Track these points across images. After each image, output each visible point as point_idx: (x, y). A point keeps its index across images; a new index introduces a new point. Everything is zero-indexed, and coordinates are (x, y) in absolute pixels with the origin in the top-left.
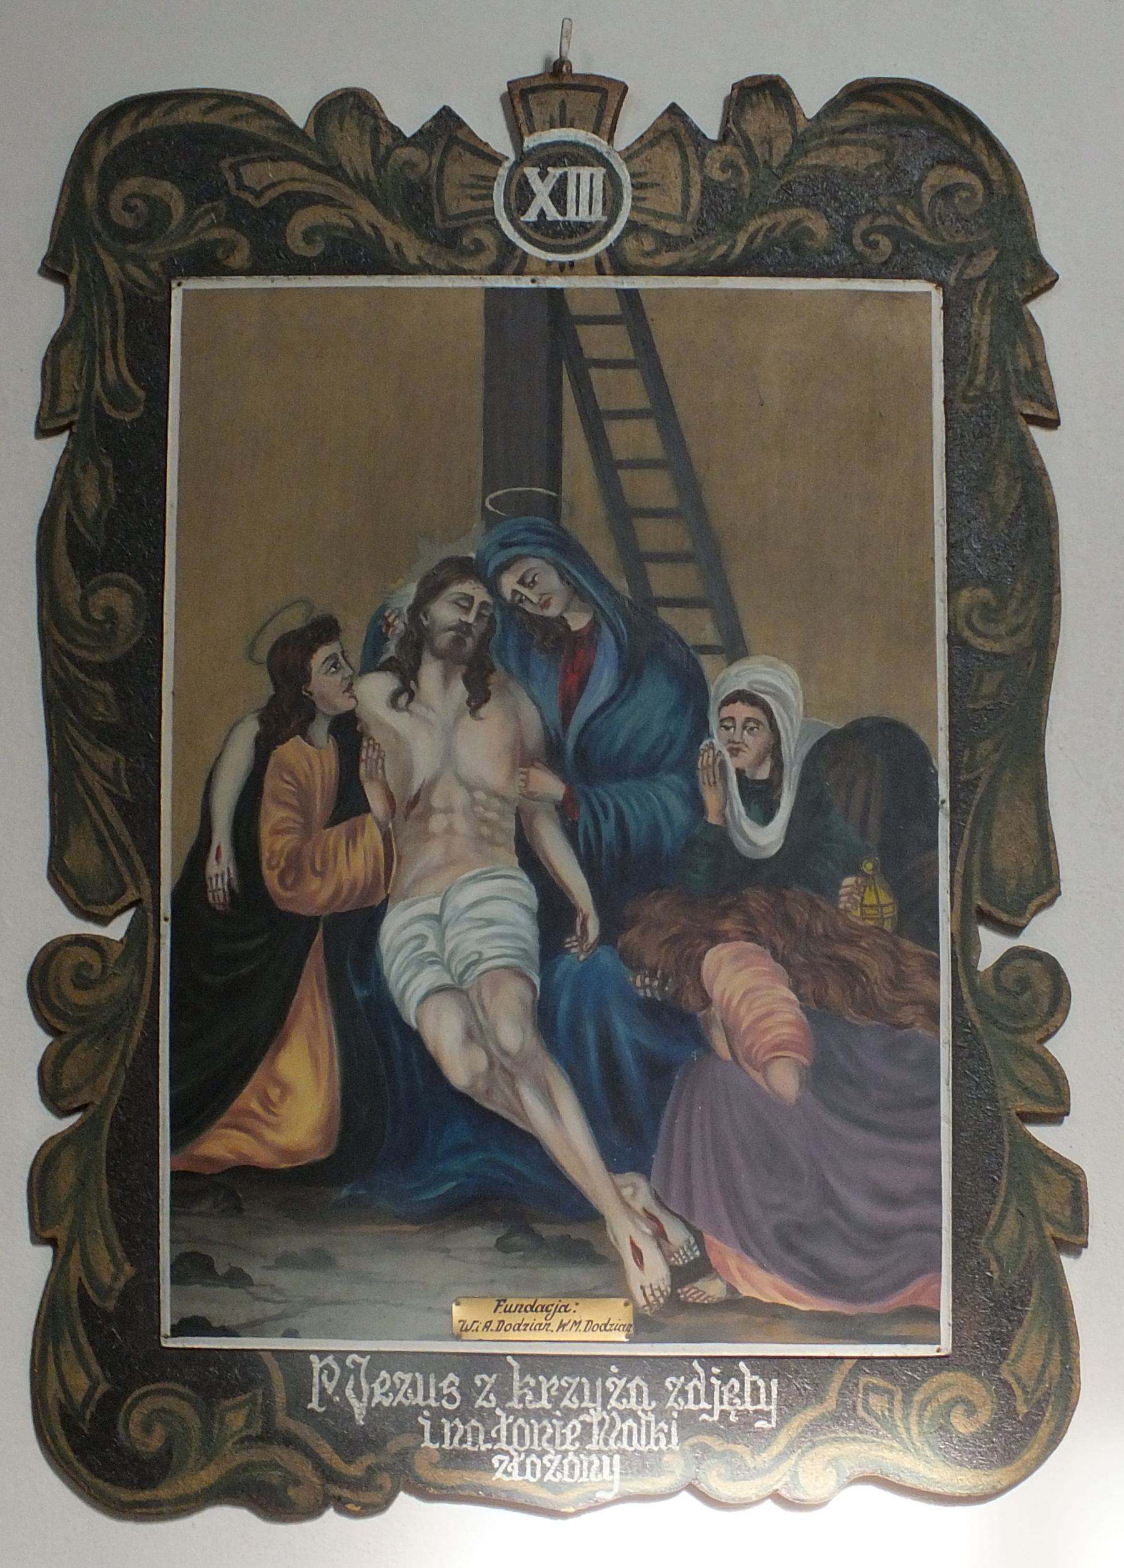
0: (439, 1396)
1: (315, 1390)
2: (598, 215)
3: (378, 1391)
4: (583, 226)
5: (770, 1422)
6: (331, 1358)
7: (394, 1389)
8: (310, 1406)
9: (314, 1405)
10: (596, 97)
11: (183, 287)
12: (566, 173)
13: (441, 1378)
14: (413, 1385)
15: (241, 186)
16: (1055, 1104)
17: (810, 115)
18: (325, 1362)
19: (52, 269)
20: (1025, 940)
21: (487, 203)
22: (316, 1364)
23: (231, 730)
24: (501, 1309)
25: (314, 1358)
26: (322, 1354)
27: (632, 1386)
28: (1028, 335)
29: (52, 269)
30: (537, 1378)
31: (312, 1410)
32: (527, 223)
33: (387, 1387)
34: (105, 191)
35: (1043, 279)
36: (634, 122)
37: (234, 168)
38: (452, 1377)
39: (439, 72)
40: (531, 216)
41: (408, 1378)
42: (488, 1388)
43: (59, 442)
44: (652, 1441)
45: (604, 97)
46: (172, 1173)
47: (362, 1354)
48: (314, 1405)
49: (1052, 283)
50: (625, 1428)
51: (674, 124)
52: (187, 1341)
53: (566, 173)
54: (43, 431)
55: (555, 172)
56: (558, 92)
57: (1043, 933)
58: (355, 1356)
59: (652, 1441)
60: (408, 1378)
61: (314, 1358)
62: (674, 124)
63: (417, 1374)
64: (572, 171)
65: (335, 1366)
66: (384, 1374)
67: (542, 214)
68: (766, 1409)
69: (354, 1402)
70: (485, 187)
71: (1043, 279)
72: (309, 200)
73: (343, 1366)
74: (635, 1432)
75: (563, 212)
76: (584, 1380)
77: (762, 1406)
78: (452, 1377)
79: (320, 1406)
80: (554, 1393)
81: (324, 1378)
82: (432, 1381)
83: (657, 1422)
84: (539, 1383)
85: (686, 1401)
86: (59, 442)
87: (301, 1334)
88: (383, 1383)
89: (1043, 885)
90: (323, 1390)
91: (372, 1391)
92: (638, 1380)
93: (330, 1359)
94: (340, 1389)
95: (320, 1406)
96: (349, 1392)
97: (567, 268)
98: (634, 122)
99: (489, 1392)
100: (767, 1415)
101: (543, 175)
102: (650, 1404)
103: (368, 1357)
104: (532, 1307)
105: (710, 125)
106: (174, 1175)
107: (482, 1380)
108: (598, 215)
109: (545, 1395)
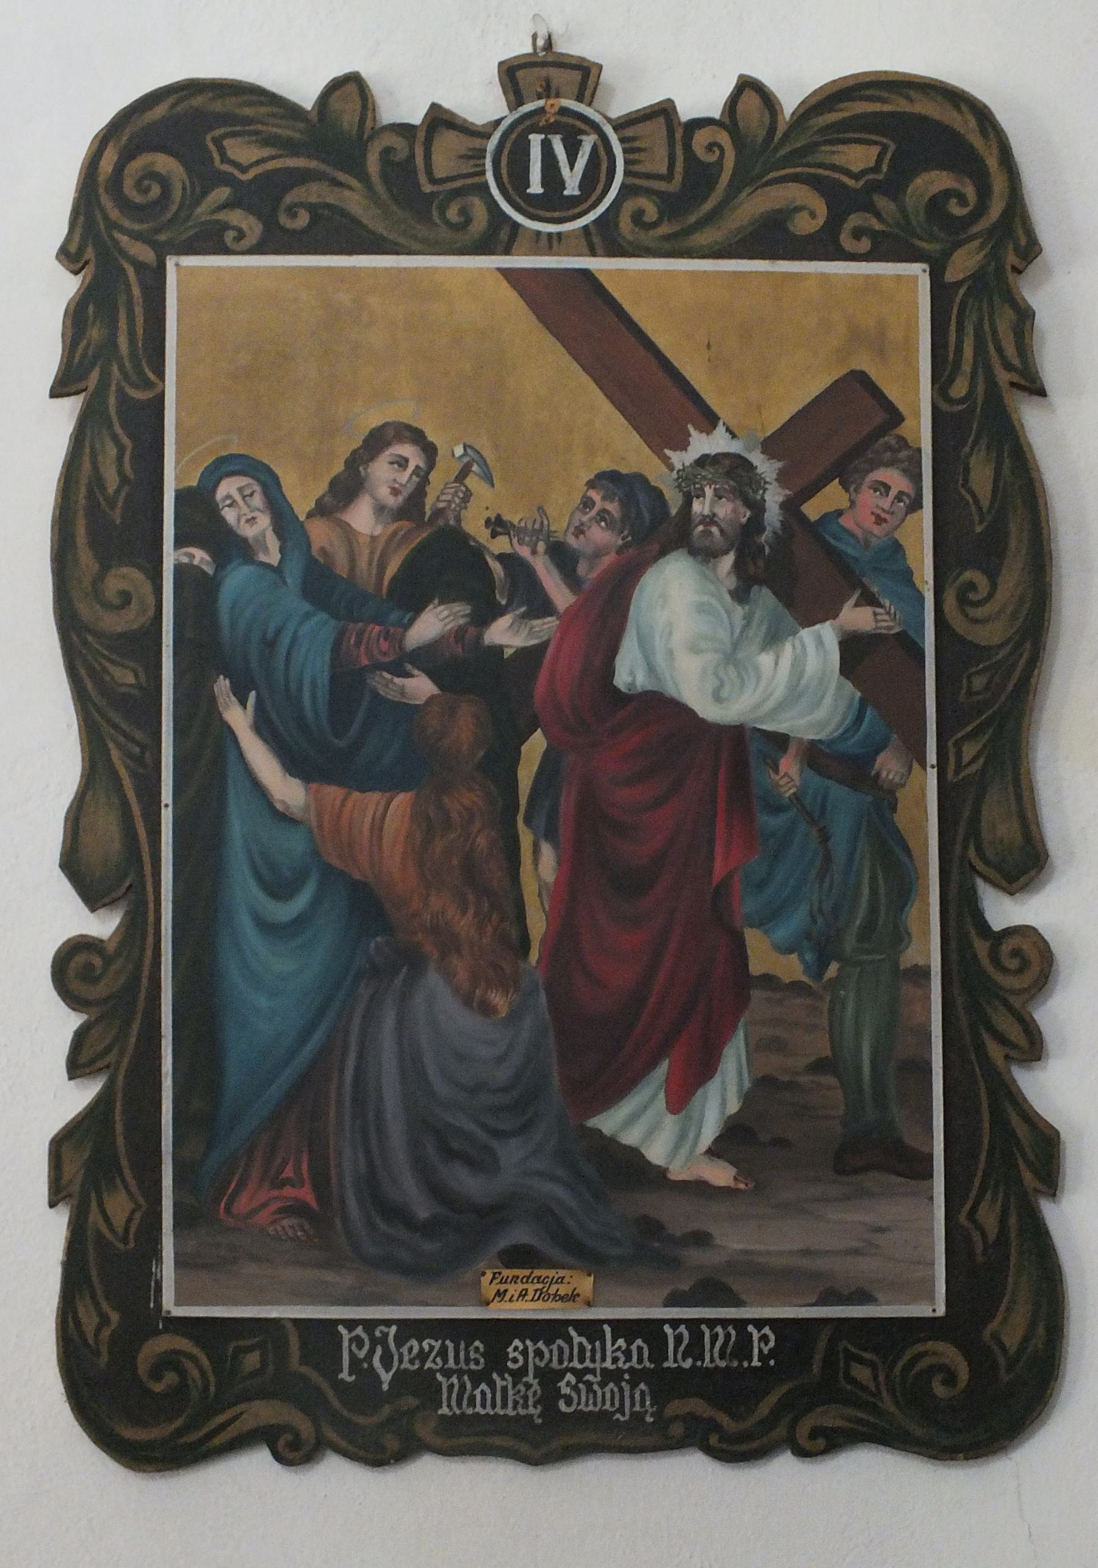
0: (468, 1360)
3: (406, 1359)
6: (360, 1328)
7: (423, 1356)
8: (666, 1365)
9: (344, 1375)
14: (443, 1353)
15: (224, 159)
18: (354, 1334)
22: (756, 1336)
24: (495, 1282)
26: (351, 1324)
29: (69, 256)
30: (524, 1343)
31: (342, 1380)
37: (218, 142)
38: (477, 1343)
41: (437, 1345)
44: (510, 1404)
45: (586, 75)
46: (932, 1176)
47: (388, 1323)
48: (344, 1375)
50: (477, 1392)
58: (383, 1328)
59: (510, 1404)
60: (437, 1345)
63: (448, 1342)
65: (364, 1336)
66: (414, 1343)
68: (591, 1366)
69: (381, 1371)
70: (479, 165)
72: (304, 177)
74: (489, 1396)
77: (588, 1363)
78: (477, 1343)
79: (350, 1374)
81: (354, 1347)
82: (462, 1345)
83: (514, 1385)
84: (526, 1348)
85: (445, 1361)
87: (879, 1296)
90: (760, 1351)
91: (401, 1356)
93: (359, 1331)
95: (350, 1374)
96: (376, 1361)
97: (544, 242)
103: (394, 1329)
104: (528, 1278)
106: (930, 1175)
107: (430, 1345)
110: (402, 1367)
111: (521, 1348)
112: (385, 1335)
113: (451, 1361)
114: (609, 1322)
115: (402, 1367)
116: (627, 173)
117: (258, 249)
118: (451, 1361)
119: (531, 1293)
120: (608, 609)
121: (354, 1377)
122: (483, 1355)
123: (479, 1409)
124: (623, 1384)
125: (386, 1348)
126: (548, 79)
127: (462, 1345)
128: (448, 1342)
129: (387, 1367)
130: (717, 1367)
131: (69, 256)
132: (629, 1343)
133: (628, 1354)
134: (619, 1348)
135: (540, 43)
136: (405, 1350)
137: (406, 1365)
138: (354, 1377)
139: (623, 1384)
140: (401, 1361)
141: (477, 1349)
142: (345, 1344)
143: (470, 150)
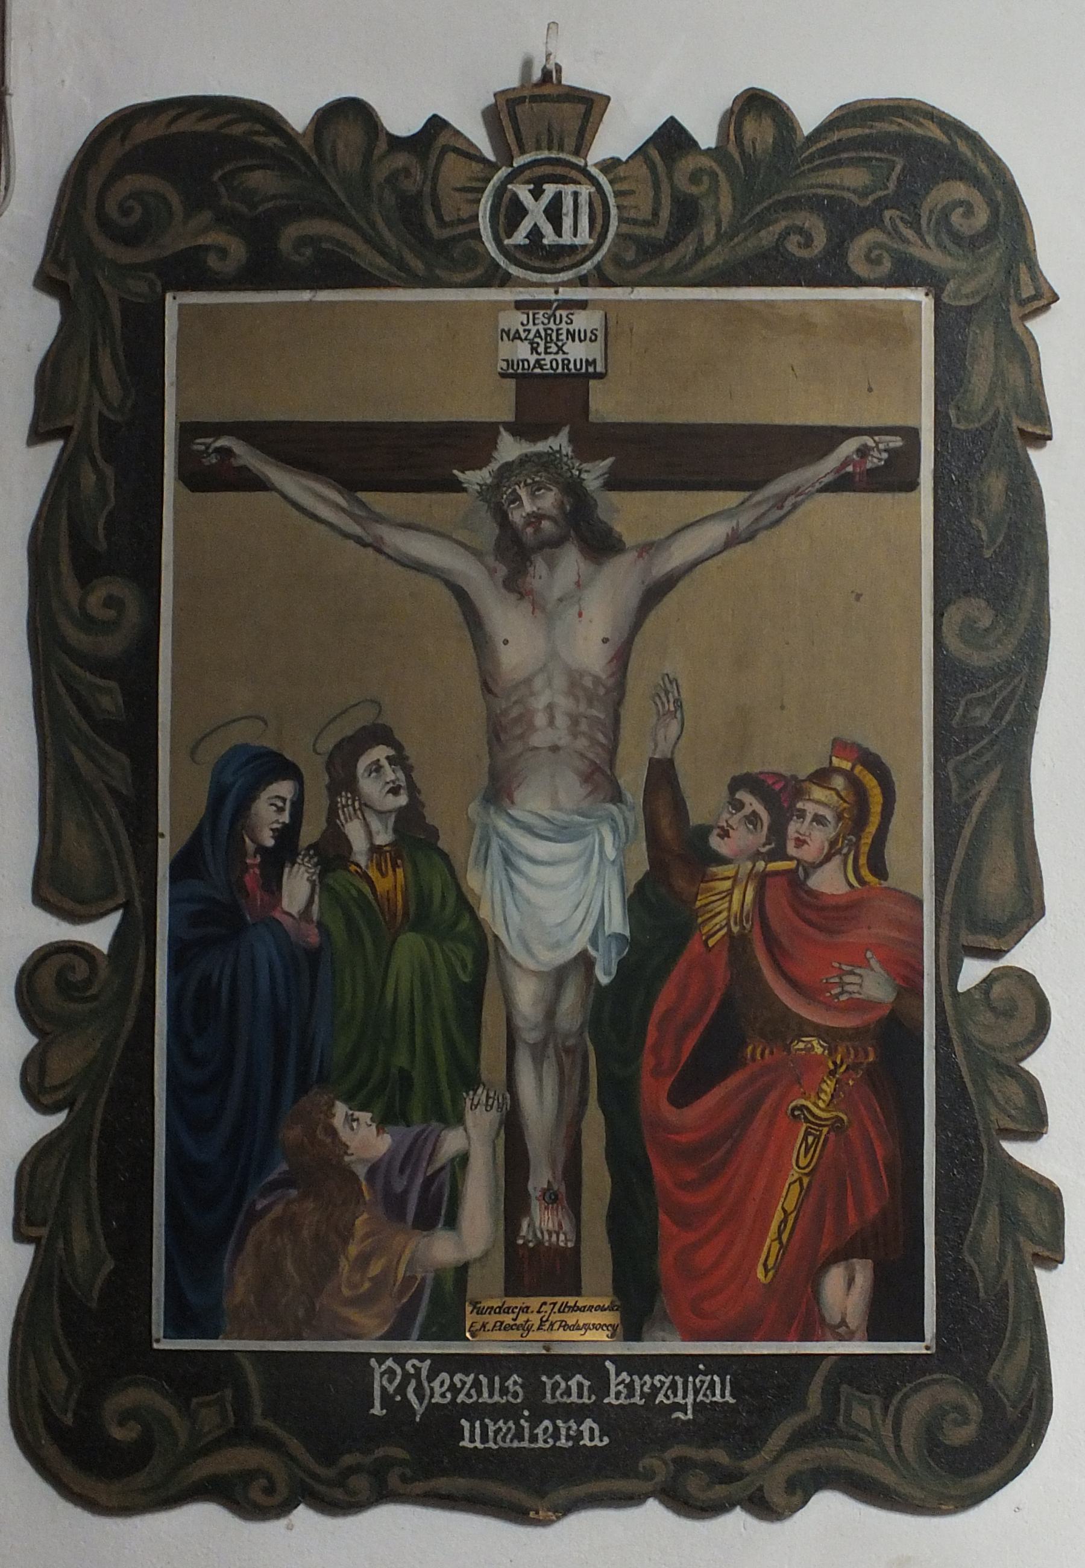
0: (504, 1391)
1: (377, 1393)
2: (584, 237)
4: (573, 248)
5: (686, 1414)
7: (655, 1391)
10: (581, 108)
11: (178, 301)
12: (560, 193)
13: (504, 1380)
16: (1033, 1122)
17: (806, 133)
18: (384, 1367)
19: (46, 282)
20: (1010, 960)
21: (472, 226)
23: (679, 531)
25: (373, 1362)
26: (381, 1358)
27: (573, 1383)
28: (1025, 355)
32: (518, 247)
33: (446, 1387)
34: (114, 177)
35: (1043, 299)
36: (617, 138)
39: (430, 81)
40: (520, 237)
41: (667, 1381)
42: (468, 1386)
43: (52, 450)
45: (590, 106)
47: (422, 1357)
48: (377, 1410)
49: (1046, 307)
51: (671, 138)
52: (449, 1347)
53: (560, 193)
54: (37, 435)
55: (550, 189)
56: (546, 113)
57: (1023, 955)
58: (415, 1362)
61: (373, 1362)
62: (671, 138)
63: (481, 1377)
64: (569, 189)
66: (444, 1376)
67: (535, 233)
68: (682, 1402)
71: (1043, 299)
73: (403, 1368)
75: (558, 232)
76: (716, 1378)
77: (679, 1399)
80: (646, 1389)
81: (385, 1383)
85: (480, 1394)
86: (52, 450)
88: (442, 1384)
89: (1028, 907)
90: (383, 1389)
92: (579, 1377)
93: (390, 1362)
94: (402, 1389)
98: (617, 138)
99: (471, 1388)
100: (683, 1408)
101: (537, 194)
102: (589, 1398)
103: (428, 1362)
105: (706, 137)
107: (660, 1381)
108: (584, 237)
109: (638, 1393)
110: (433, 1401)
111: (628, 1380)
112: (418, 1370)
113: (486, 1394)
114: (613, 1358)
115: (433, 1401)
116: (621, 220)
117: (946, 668)
118: (486, 1394)
119: (489, 1327)
120: (831, 762)
121: (384, 1411)
122: (522, 1386)
123: (491, 1444)
124: (522, 1421)
125: (419, 1384)
126: (546, 113)
127: (497, 1379)
128: (716, 1378)
129: (421, 1399)
130: (727, 1402)
131: (47, 281)
132: (567, 1379)
133: (630, 1387)
134: (623, 1381)
135: (537, 75)
136: (436, 1384)
137: (436, 1399)
138: (384, 1411)
139: (522, 1421)
140: (432, 1396)
141: (515, 1383)
142: (377, 1376)
143: (471, 179)
